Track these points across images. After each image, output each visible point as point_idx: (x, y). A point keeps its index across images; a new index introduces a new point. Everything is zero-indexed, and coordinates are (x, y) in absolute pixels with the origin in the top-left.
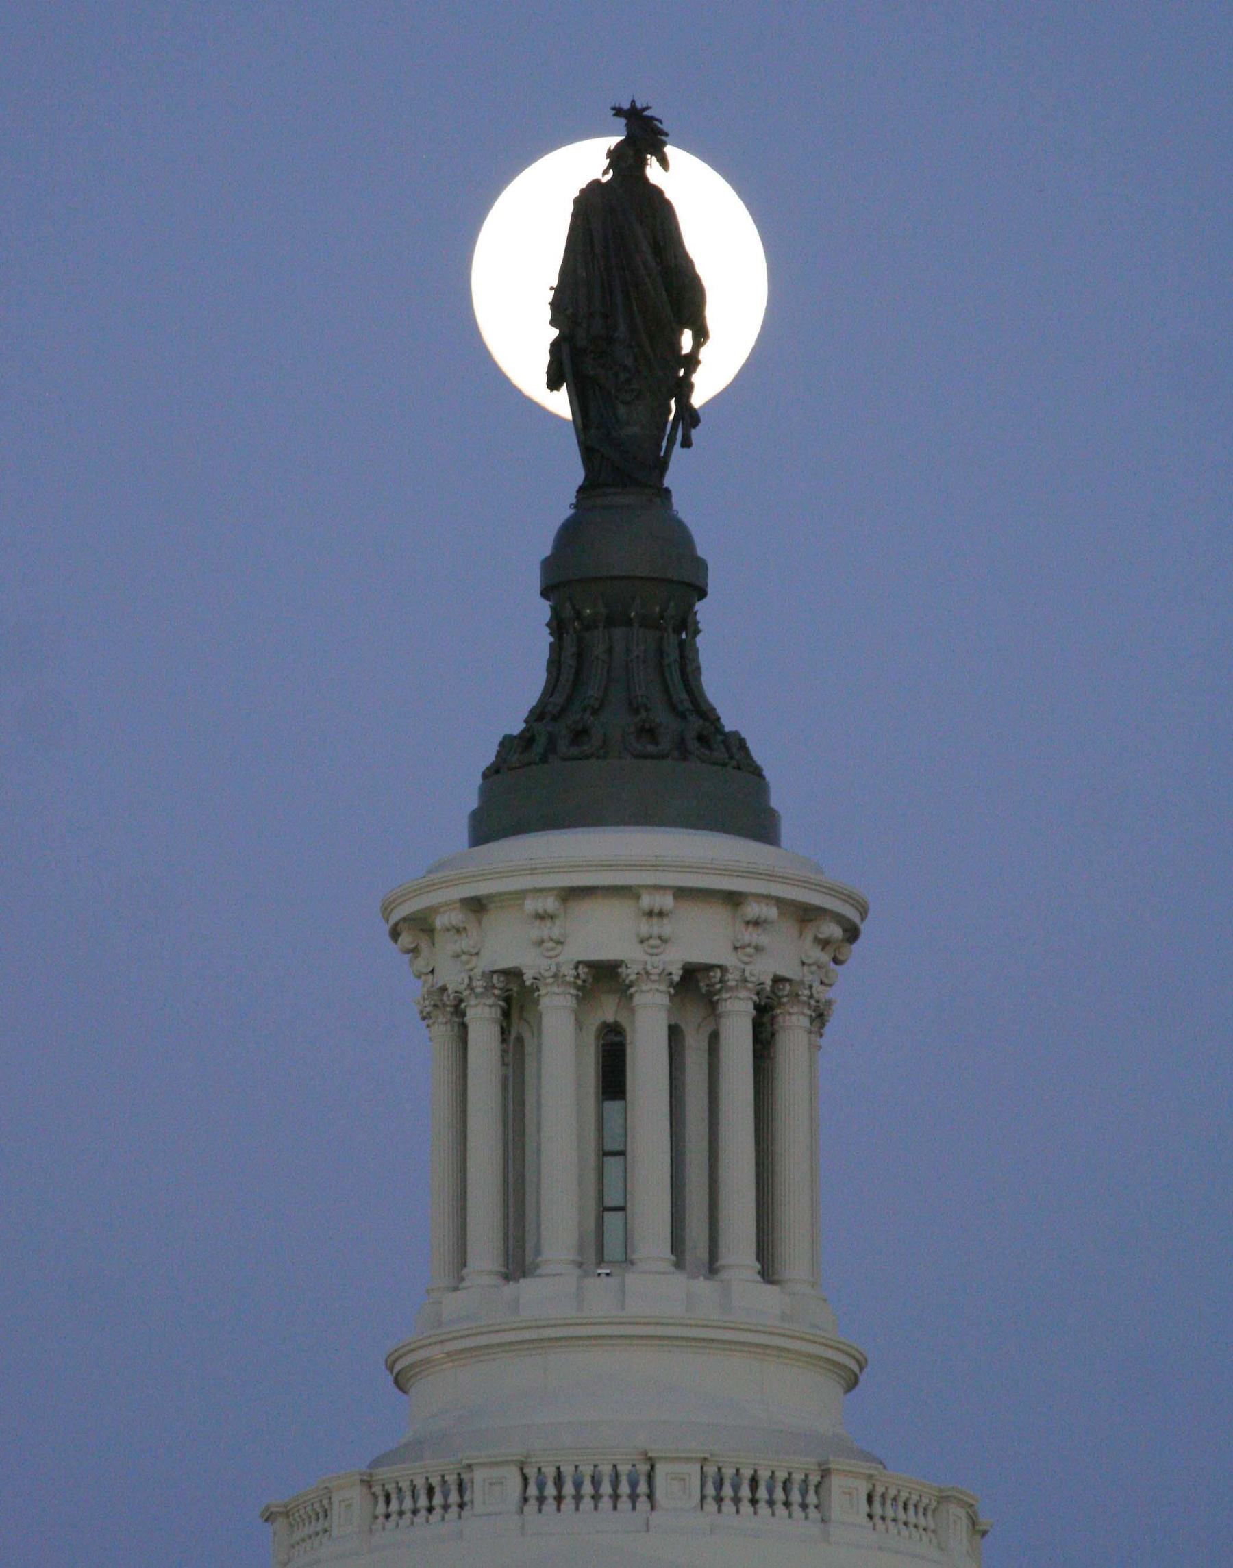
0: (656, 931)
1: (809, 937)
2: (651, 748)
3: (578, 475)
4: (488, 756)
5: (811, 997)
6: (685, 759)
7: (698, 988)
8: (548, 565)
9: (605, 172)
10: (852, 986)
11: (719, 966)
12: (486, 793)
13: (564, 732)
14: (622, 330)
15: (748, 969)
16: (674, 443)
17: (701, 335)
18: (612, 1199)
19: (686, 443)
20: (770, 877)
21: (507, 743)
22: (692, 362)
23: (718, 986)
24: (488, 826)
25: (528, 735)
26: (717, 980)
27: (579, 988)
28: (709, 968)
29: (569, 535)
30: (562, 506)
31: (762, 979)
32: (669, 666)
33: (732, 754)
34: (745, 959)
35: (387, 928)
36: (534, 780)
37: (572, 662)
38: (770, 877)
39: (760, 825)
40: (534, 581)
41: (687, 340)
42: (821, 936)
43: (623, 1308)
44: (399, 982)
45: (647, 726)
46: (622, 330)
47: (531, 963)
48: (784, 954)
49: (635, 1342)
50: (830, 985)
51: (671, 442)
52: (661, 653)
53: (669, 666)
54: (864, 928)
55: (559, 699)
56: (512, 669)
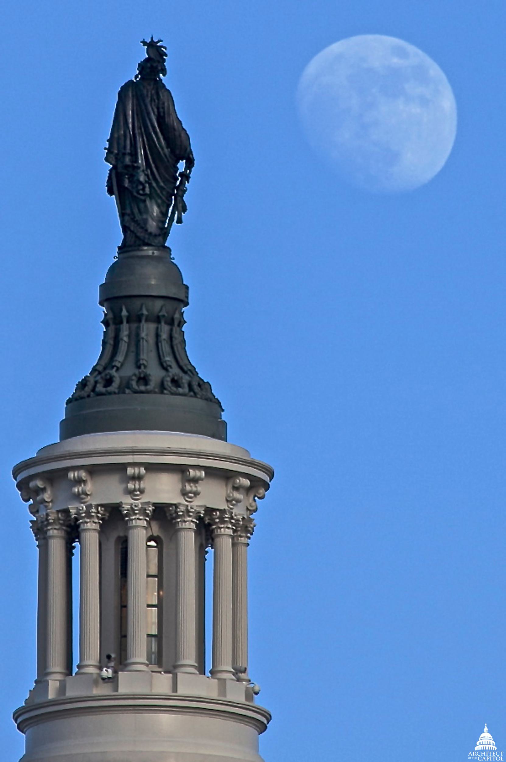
1: (230, 486)
2: (142, 388)
3: (119, 237)
5: (232, 518)
6: (162, 393)
7: (166, 517)
11: (175, 504)
13: (100, 380)
15: (234, 511)
16: (173, 221)
17: (190, 163)
18: (123, 634)
19: (180, 221)
20: (199, 455)
22: (185, 177)
23: (174, 515)
25: (84, 382)
26: (173, 512)
28: (171, 505)
30: (112, 256)
32: (176, 345)
34: (231, 507)
38: (199, 455)
39: (219, 431)
42: (236, 486)
43: (117, 691)
45: (142, 376)
49: (136, 708)
51: (171, 220)
52: (157, 336)
53: (176, 345)
55: (103, 363)
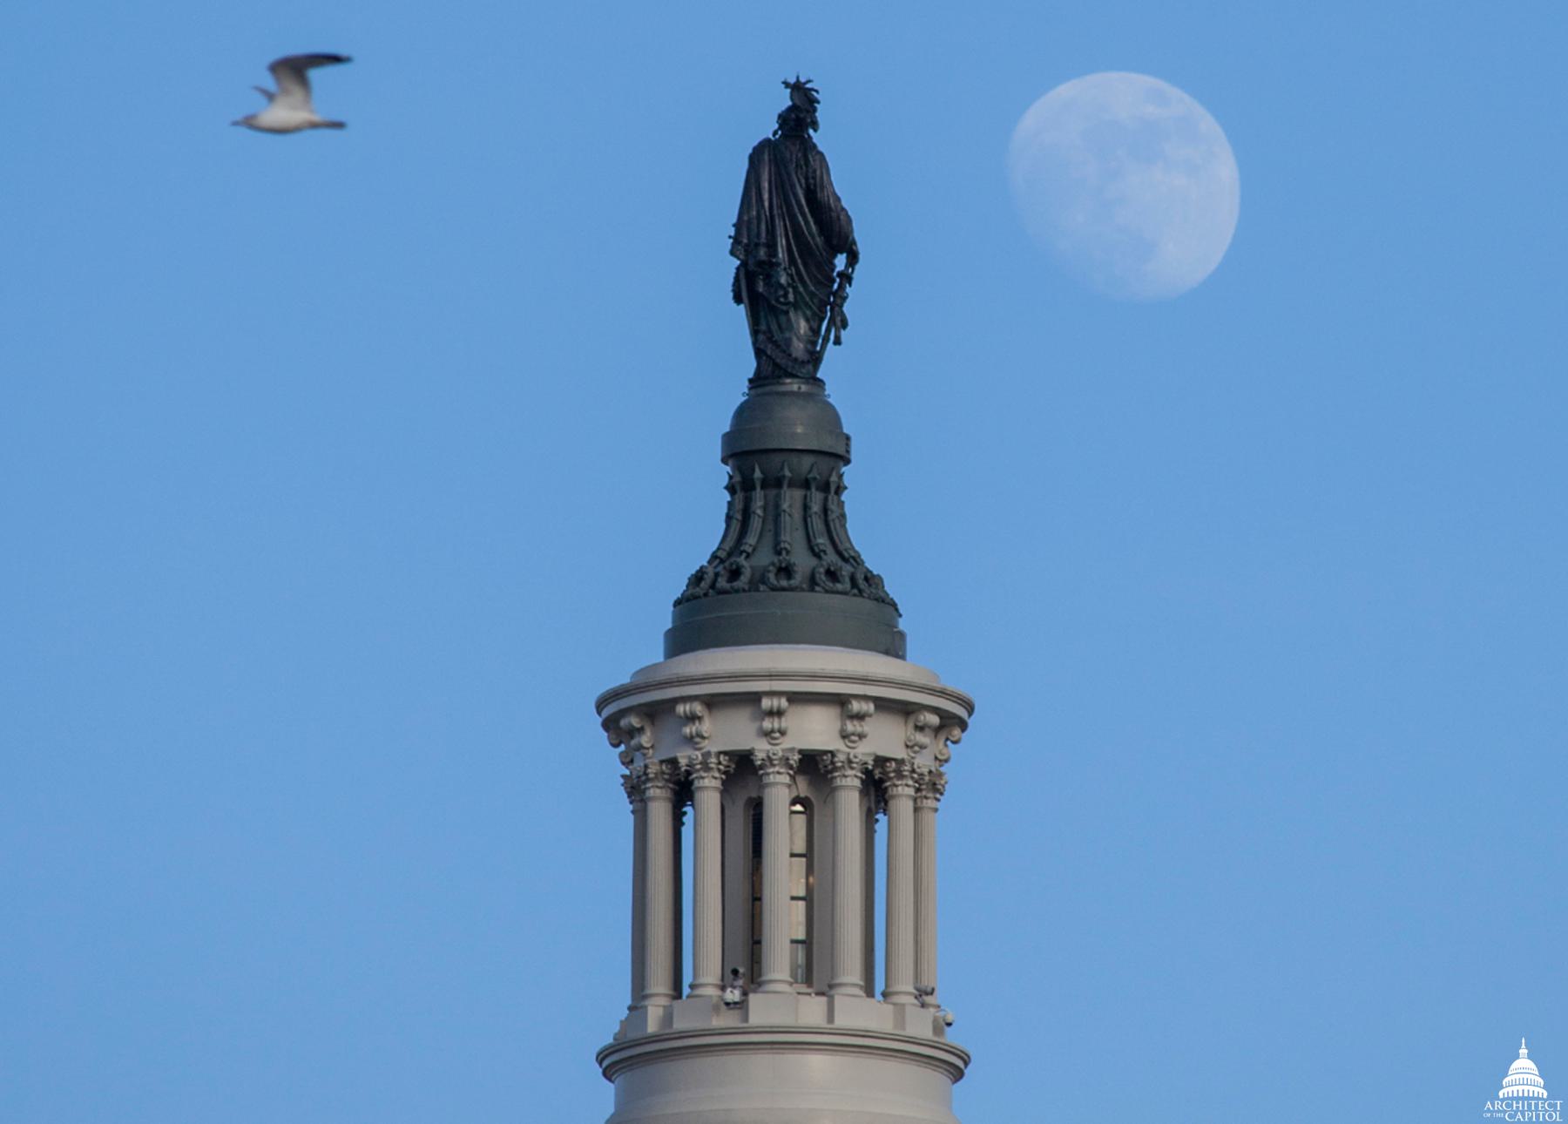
0: (776, 726)
1: (911, 725)
2: (784, 583)
3: (749, 365)
4: (679, 587)
5: (913, 771)
6: (812, 590)
8: (728, 439)
9: (775, 133)
10: (964, 761)
12: (677, 617)
14: (781, 254)
17: (853, 258)
19: (838, 342)
21: (698, 578)
24: (682, 640)
27: (725, 773)
28: (826, 752)
29: (741, 414)
30: (738, 393)
31: (865, 759)
33: (866, 585)
35: (600, 720)
36: (712, 607)
37: (739, 517)
38: (865, 680)
40: (717, 451)
41: (840, 262)
44: (609, 763)
46: (781, 254)
47: (761, 748)
48: (884, 738)
50: (946, 761)
51: (826, 340)
52: (806, 507)
54: (970, 721)
56: (696, 518)
